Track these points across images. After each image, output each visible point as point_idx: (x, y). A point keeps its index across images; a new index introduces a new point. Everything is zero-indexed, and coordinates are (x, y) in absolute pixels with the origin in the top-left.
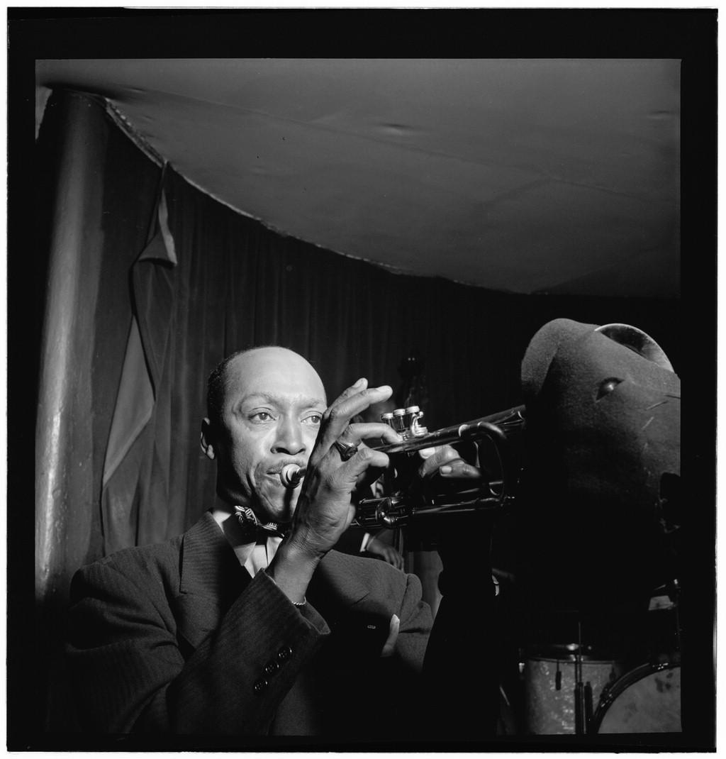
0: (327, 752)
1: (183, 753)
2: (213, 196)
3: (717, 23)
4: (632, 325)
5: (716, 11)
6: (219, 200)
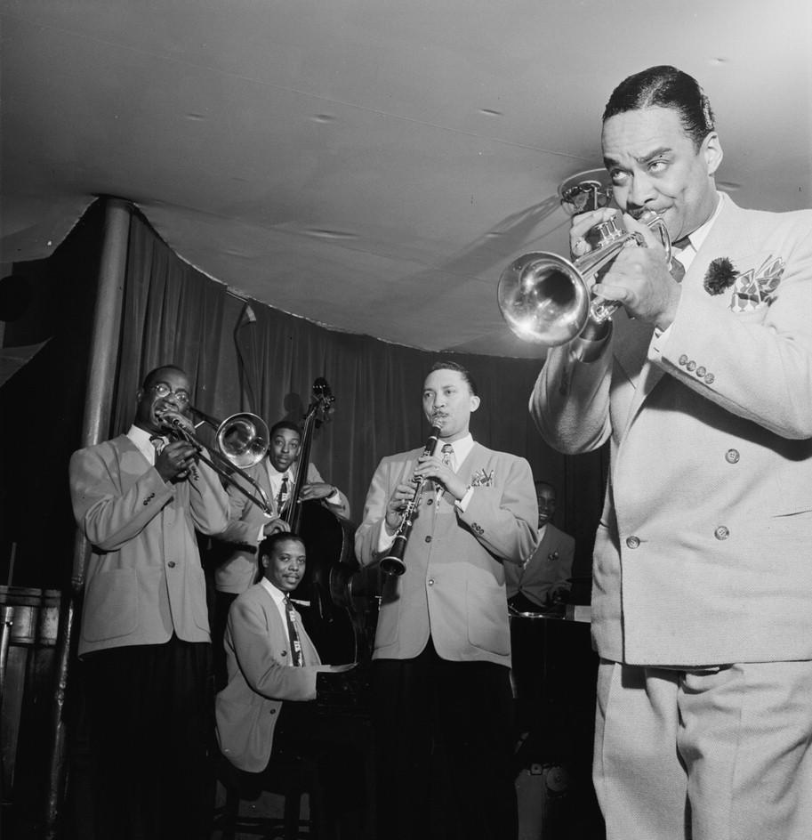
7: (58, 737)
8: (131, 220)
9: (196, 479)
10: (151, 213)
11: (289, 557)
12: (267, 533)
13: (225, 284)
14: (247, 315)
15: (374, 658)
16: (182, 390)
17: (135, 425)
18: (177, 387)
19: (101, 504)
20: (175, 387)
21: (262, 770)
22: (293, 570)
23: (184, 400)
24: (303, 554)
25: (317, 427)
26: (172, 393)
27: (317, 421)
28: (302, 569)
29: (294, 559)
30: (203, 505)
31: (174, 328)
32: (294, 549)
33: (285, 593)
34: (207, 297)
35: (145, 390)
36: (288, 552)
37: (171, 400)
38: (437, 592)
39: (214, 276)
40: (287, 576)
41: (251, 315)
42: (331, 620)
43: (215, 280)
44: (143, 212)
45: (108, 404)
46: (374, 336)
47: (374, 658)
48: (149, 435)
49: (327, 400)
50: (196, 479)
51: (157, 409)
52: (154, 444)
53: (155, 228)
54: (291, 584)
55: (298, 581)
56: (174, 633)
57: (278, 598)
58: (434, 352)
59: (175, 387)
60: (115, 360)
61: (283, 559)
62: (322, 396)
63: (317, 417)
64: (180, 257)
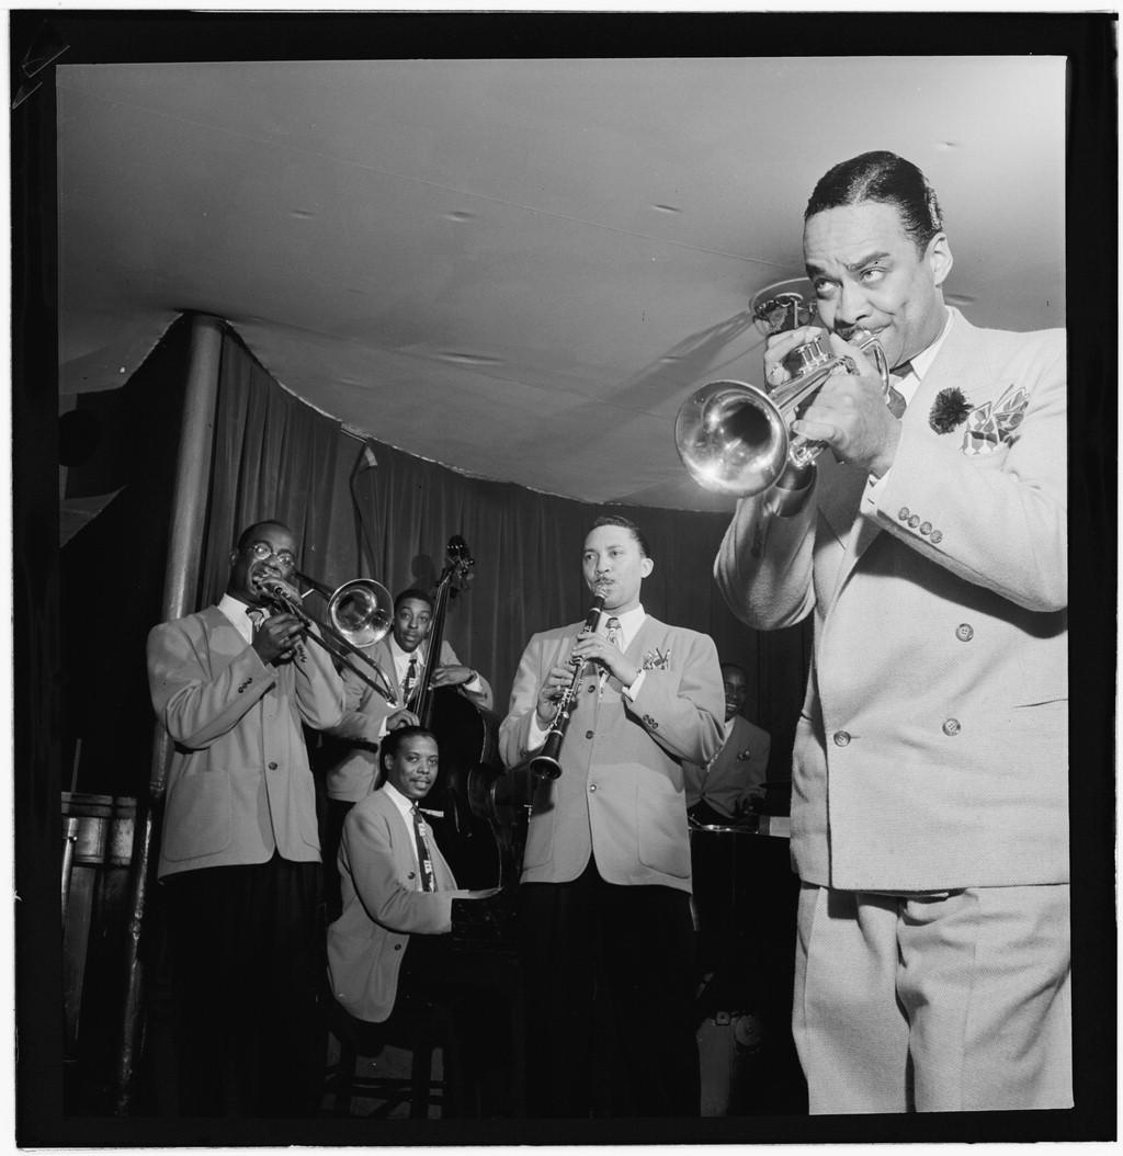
7: (132, 979)
8: (223, 341)
9: (303, 661)
10: (247, 333)
11: (418, 756)
12: (391, 727)
13: (339, 420)
14: (366, 459)
15: (522, 881)
16: (286, 551)
17: (228, 594)
18: (280, 547)
19: (185, 691)
20: (277, 547)
21: (384, 1019)
22: (423, 773)
23: (289, 563)
24: (436, 753)
25: (453, 596)
26: (274, 555)
27: (452, 589)
28: (434, 772)
29: (424, 759)
30: (311, 693)
31: (276, 475)
32: (424, 746)
33: (413, 801)
34: (317, 437)
35: (241, 551)
36: (417, 751)
37: (272, 564)
38: (600, 800)
39: (325, 410)
40: (415, 780)
41: (371, 458)
42: (470, 835)
43: (327, 415)
44: (238, 331)
45: (194, 568)
46: (523, 485)
48: (245, 607)
49: (464, 563)
50: (303, 661)
51: (255, 574)
52: (251, 617)
53: (253, 352)
54: (421, 789)
55: (429, 786)
56: (276, 851)
57: (405, 807)
58: (596, 505)
59: (277, 547)
60: (203, 513)
61: (410, 759)
62: (459, 558)
63: (452, 585)
64: (284, 387)
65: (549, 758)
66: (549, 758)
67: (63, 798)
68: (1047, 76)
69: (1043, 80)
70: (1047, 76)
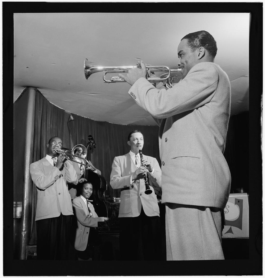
0: (66, 275)
1: (85, 276)
2: (55, 105)
3: (263, 8)
4: (225, 149)
5: (263, 3)
6: (56, 106)
7: (23, 245)
8: (36, 93)
9: (67, 167)
10: (41, 91)
11: (88, 188)
12: (79, 182)
13: (64, 109)
14: (71, 118)
15: (119, 217)
16: (60, 143)
17: (47, 154)
18: (59, 142)
19: (40, 178)
20: (58, 142)
21: (85, 250)
22: (89, 192)
23: (61, 145)
24: (92, 188)
25: (90, 149)
26: (57, 144)
27: (90, 148)
28: (91, 192)
29: (89, 189)
30: (69, 174)
31: (50, 123)
32: (89, 186)
33: (87, 199)
34: (59, 113)
35: (49, 144)
36: (88, 187)
37: (57, 146)
38: (143, 197)
39: (61, 107)
40: (87, 194)
41: (72, 118)
42: (97, 204)
43: (61, 108)
44: (40, 91)
45: (32, 147)
46: (108, 122)
47: (119, 217)
48: (51, 157)
49: (92, 141)
50: (67, 167)
51: (53, 148)
52: (53, 159)
53: (43, 95)
54: (88, 196)
55: (90, 195)
56: (61, 213)
57: (85, 200)
58: (125, 125)
59: (58, 142)
60: (33, 134)
61: (86, 189)
62: (91, 140)
63: (90, 147)
64: (51, 103)
65: (148, 190)
66: (148, 190)
67: (14, 203)
68: (245, 17)
69: (244, 19)
70: (245, 17)
